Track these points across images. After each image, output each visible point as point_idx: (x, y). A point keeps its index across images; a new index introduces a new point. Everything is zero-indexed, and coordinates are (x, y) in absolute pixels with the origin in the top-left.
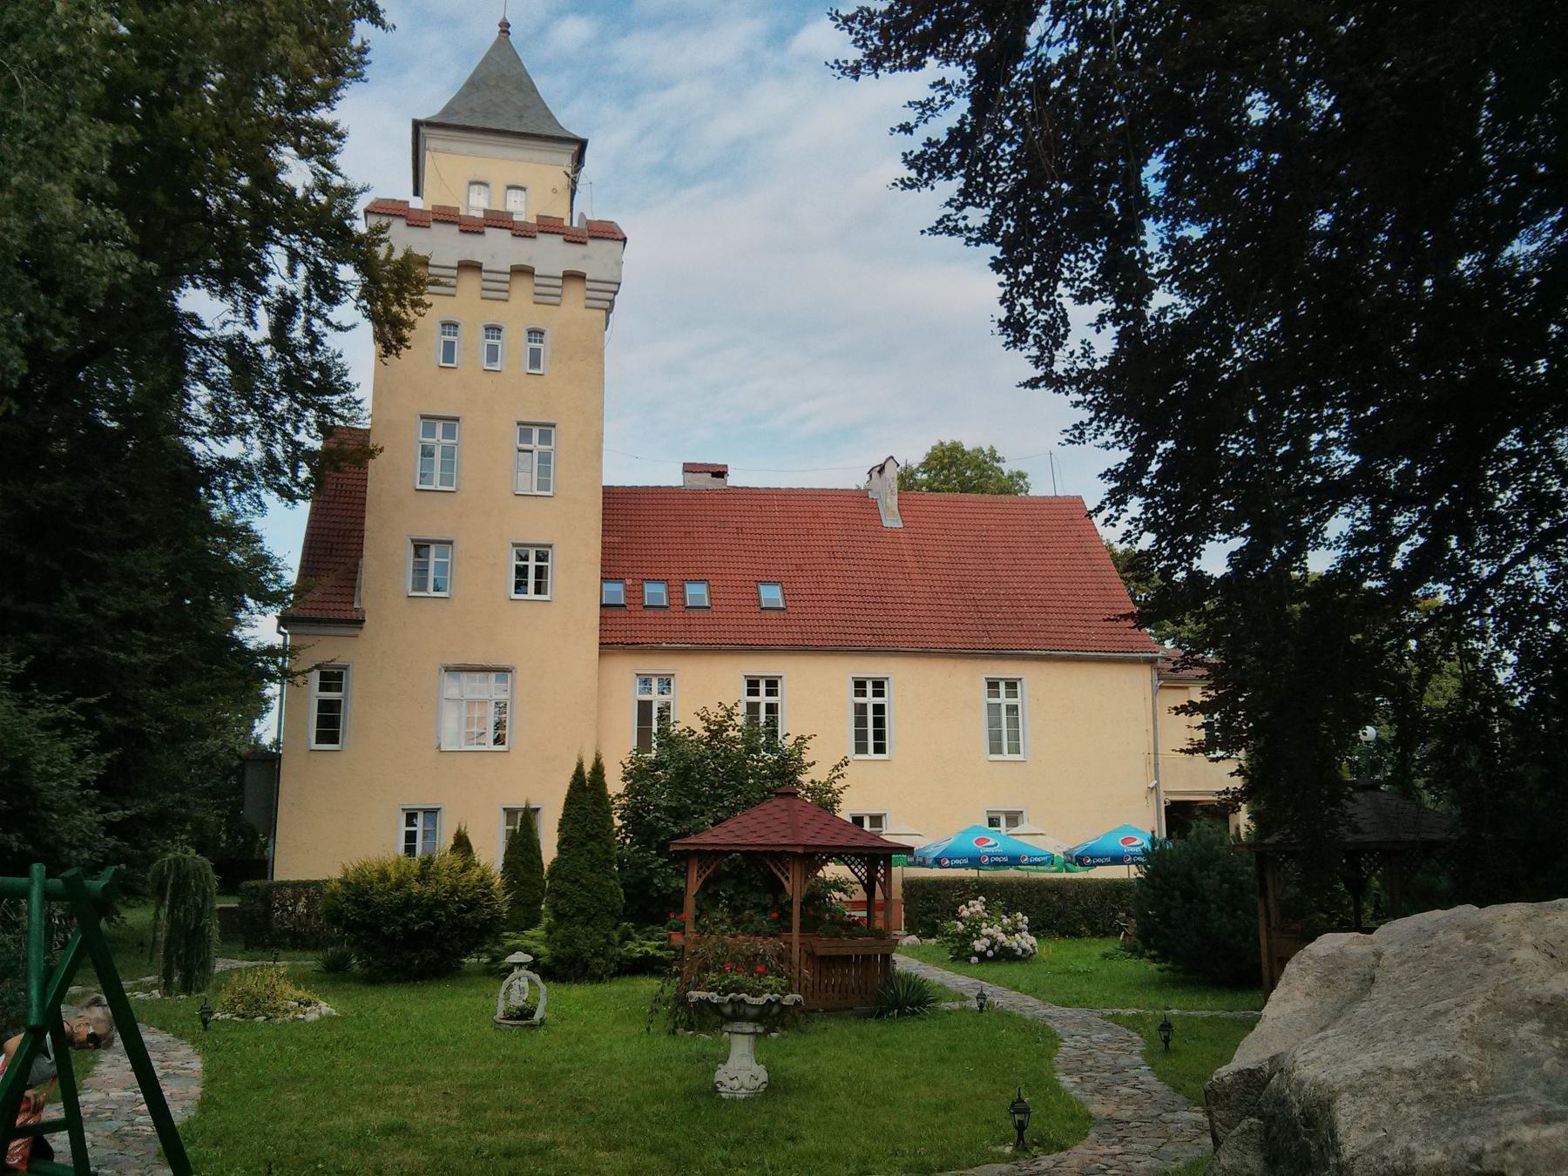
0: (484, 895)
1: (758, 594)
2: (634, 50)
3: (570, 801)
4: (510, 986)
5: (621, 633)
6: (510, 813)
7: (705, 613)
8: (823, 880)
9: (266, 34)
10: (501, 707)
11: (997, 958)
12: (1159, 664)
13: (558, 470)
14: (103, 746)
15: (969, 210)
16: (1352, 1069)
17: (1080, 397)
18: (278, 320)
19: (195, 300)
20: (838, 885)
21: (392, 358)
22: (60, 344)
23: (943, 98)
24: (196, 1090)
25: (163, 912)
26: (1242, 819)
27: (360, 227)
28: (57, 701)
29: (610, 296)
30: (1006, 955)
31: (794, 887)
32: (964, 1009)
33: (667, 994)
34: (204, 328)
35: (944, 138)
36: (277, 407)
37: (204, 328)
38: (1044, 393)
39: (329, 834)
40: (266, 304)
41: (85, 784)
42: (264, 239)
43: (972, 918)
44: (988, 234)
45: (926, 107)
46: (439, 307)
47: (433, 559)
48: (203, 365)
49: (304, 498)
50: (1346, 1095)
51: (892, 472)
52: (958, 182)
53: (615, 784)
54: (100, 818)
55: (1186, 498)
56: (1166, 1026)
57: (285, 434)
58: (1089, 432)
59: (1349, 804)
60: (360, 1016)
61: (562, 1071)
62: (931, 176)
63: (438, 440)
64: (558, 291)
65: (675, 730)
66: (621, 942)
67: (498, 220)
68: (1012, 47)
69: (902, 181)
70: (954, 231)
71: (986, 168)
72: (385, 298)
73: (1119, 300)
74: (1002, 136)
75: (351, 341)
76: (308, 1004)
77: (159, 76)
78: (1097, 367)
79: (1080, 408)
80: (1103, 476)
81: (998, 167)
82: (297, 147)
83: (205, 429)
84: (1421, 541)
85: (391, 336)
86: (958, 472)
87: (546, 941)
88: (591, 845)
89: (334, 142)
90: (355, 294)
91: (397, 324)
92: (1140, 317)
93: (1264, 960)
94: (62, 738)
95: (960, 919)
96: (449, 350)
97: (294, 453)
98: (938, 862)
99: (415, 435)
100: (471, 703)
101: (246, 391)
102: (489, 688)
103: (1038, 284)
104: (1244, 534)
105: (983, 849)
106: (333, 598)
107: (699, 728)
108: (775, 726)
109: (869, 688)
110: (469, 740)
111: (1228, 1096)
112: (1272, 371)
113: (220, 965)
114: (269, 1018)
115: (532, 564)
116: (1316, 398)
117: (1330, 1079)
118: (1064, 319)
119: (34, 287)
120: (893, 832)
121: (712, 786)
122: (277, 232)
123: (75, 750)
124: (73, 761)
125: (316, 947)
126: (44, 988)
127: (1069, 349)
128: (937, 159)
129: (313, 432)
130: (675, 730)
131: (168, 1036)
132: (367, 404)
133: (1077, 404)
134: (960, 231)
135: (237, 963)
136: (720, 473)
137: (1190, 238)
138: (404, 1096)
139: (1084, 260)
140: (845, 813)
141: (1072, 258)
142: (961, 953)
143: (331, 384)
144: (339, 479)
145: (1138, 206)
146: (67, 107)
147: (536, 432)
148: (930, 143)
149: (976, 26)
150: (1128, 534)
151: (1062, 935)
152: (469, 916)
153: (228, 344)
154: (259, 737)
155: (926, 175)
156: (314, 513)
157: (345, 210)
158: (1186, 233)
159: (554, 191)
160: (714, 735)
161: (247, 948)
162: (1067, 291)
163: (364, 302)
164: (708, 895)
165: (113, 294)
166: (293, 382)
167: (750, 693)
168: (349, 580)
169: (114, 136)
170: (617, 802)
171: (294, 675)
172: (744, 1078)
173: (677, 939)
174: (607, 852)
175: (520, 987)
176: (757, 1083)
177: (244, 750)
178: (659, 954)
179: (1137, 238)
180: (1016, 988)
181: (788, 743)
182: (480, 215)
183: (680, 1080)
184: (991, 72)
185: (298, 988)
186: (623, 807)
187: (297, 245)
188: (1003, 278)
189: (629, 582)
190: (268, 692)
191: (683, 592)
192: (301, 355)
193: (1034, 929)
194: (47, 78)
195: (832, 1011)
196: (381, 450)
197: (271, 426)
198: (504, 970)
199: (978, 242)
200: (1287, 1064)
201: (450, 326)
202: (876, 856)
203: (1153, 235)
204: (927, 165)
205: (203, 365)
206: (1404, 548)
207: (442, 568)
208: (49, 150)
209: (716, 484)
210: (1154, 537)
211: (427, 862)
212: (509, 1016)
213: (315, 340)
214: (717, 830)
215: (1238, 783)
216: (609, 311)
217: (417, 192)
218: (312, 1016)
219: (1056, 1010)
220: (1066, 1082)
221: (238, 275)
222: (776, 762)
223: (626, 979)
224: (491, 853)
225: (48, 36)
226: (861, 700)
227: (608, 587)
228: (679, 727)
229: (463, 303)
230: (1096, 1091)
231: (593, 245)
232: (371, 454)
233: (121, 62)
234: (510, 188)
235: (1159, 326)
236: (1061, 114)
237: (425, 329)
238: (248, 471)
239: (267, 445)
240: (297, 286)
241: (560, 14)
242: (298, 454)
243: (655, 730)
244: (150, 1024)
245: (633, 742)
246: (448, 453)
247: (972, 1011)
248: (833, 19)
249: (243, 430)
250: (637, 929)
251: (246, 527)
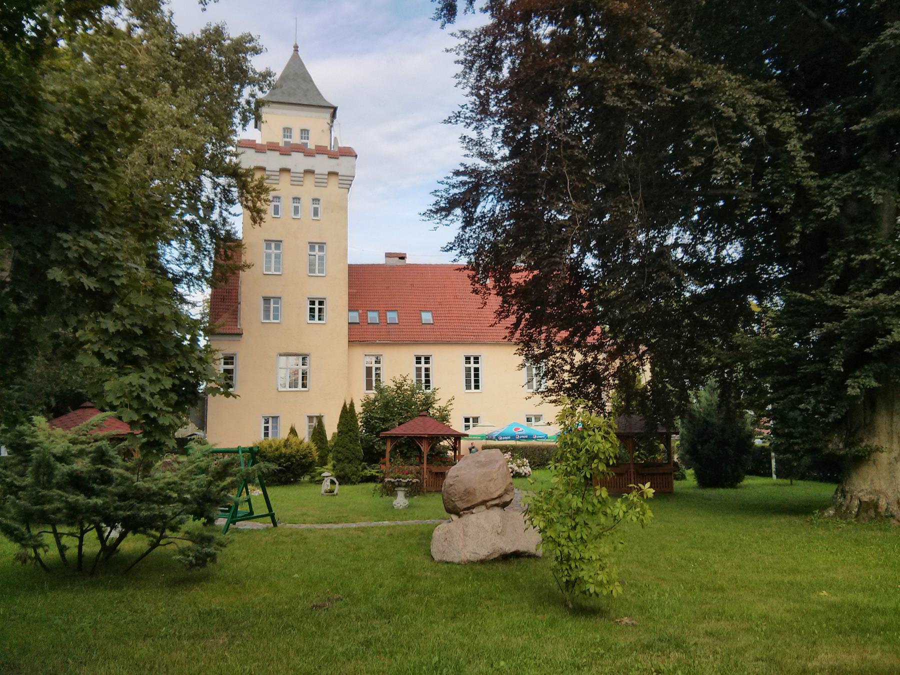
5: (358, 336)
6: (311, 418)
7: (396, 326)
31: (425, 448)
47: (272, 305)
53: (358, 409)
65: (382, 385)
88: (350, 433)
98: (497, 438)
105: (517, 433)
107: (392, 385)
136: (402, 257)
160: (399, 388)
168: (235, 314)
172: (402, 503)
173: (383, 467)
207: (276, 310)
224: (304, 434)
226: (468, 365)
231: (342, 159)
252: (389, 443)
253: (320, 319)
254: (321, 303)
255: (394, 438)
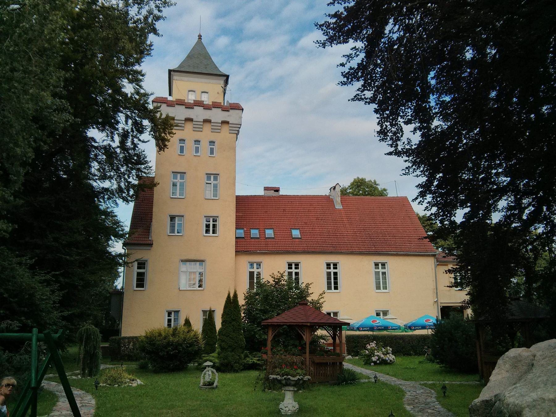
0: (196, 341)
1: (291, 233)
2: (244, 47)
3: (226, 307)
4: (205, 374)
5: (243, 247)
6: (205, 312)
7: (273, 240)
8: (317, 336)
9: (117, 39)
10: (201, 274)
11: (380, 364)
12: (437, 256)
13: (221, 190)
14: (61, 289)
15: (366, 92)
16: (528, 399)
17: (407, 159)
18: (122, 139)
19: (93, 133)
20: (322, 337)
21: (162, 152)
22: (46, 147)
23: (355, 53)
24: (93, 411)
25: (82, 348)
26: (469, 312)
27: (151, 107)
28: (45, 273)
29: (238, 129)
30: (384, 362)
31: (306, 338)
32: (369, 382)
33: (261, 377)
34: (97, 142)
35: (356, 67)
36: (122, 170)
37: (97, 142)
38: (394, 157)
39: (141, 320)
40: (118, 134)
41: (54, 302)
42: (116, 110)
43: (371, 349)
44: (373, 100)
45: (349, 57)
46: (178, 134)
48: (96, 155)
49: (132, 201)
50: (527, 409)
51: (338, 189)
52: (362, 82)
53: (241, 301)
54: (60, 314)
55: (447, 194)
56: (444, 387)
57: (125, 179)
58: (411, 170)
59: (510, 305)
60: (152, 385)
61: (224, 404)
62: (352, 80)
63: (178, 180)
64: (220, 128)
65: (263, 281)
66: (244, 358)
67: (198, 103)
68: (379, 33)
69: (341, 82)
70: (359, 100)
71: (371, 77)
72: (159, 131)
73: (421, 122)
74: (376, 65)
75: (148, 146)
76: (133, 380)
77: (79, 56)
78: (413, 147)
79: (407, 162)
80: (417, 186)
81: (376, 77)
82: (128, 79)
83: (97, 178)
84: (533, 209)
85: (162, 144)
86: (363, 189)
87: (218, 358)
88: (234, 323)
89: (141, 77)
90: (149, 130)
91: (164, 140)
92: (429, 128)
93: (479, 362)
94: (47, 286)
95: (367, 350)
96: (182, 149)
97: (128, 185)
98: (358, 329)
99: (171, 179)
100: (190, 273)
101: (112, 164)
102: (197, 268)
103: (391, 118)
104: (469, 207)
105: (374, 324)
106: (142, 236)
108: (298, 280)
109: (332, 266)
110: (190, 286)
111: (478, 410)
112: (477, 149)
113: (102, 367)
114: (119, 385)
115: (211, 223)
116: (493, 157)
117: (520, 403)
118: (401, 129)
119: (37, 127)
120: (342, 317)
121: (276, 302)
122: (121, 109)
123: (51, 291)
124: (50, 294)
125: (137, 360)
126: (37, 372)
127: (403, 141)
128: (353, 74)
129: (135, 178)
130: (263, 281)
131: (83, 392)
132: (154, 168)
133: (406, 161)
134: (363, 99)
135: (108, 366)
136: (277, 190)
137: (446, 101)
138: (167, 413)
139: (408, 109)
140: (325, 310)
141: (403, 108)
142: (368, 362)
143: (141, 161)
144: (144, 194)
145: (427, 90)
146: (49, 65)
147: (212, 177)
148: (351, 68)
149: (367, 28)
150: (427, 208)
151: (404, 355)
152: (190, 349)
153: (105, 148)
154: (116, 286)
155: (350, 80)
156: (135, 206)
157: (145, 101)
158: (444, 99)
159: (218, 93)
160: (277, 283)
161: (112, 361)
162: (402, 120)
163: (152, 133)
164: (275, 341)
165: (65, 130)
166: (127, 160)
167: (289, 268)
169: (64, 75)
170: (242, 308)
171: (128, 263)
173: (265, 357)
174: (239, 325)
175: (209, 374)
176: (295, 409)
177: (111, 290)
178: (258, 362)
179: (427, 100)
180: (388, 374)
181: (303, 286)
182: (192, 102)
183: (267, 408)
184: (372, 44)
185: (130, 375)
186: (245, 309)
187: (129, 113)
188: (378, 116)
189: (245, 229)
190: (119, 270)
191: (265, 233)
192: (130, 151)
193: (394, 353)
194: (41, 56)
195: (321, 383)
196: (159, 184)
197: (120, 176)
198: (203, 368)
199: (369, 103)
200: (502, 397)
201: (182, 141)
202: (336, 326)
203: (432, 100)
204: (350, 77)
205: (96, 155)
206: (527, 212)
207: (180, 225)
208: (42, 80)
209: (276, 194)
210: (436, 208)
211: (175, 329)
212: (205, 385)
213: (135, 146)
214: (278, 317)
215: (468, 298)
216: (237, 134)
217: (170, 95)
218: (134, 385)
219: (403, 382)
220: (408, 408)
221: (108, 123)
222: (299, 293)
223: (247, 371)
224: (198, 326)
225: (42, 41)
226: (329, 270)
227: (238, 231)
228: (264, 280)
229: (187, 133)
230: (418, 412)
231: (232, 111)
232: (155, 185)
233: (67, 50)
234: (202, 92)
235: (436, 132)
236: (398, 58)
237: (174, 141)
238: (112, 193)
239: (119, 183)
240: (129, 127)
241: (219, 36)
242: (129, 186)
243: (255, 281)
244: (77, 387)
245: (247, 286)
246: (182, 185)
247: (372, 383)
248: (316, 26)
249: (110, 178)
250: (250, 353)
251: (112, 212)
252: (270, 333)
253: (213, 233)
254: (214, 221)
255: (275, 326)
